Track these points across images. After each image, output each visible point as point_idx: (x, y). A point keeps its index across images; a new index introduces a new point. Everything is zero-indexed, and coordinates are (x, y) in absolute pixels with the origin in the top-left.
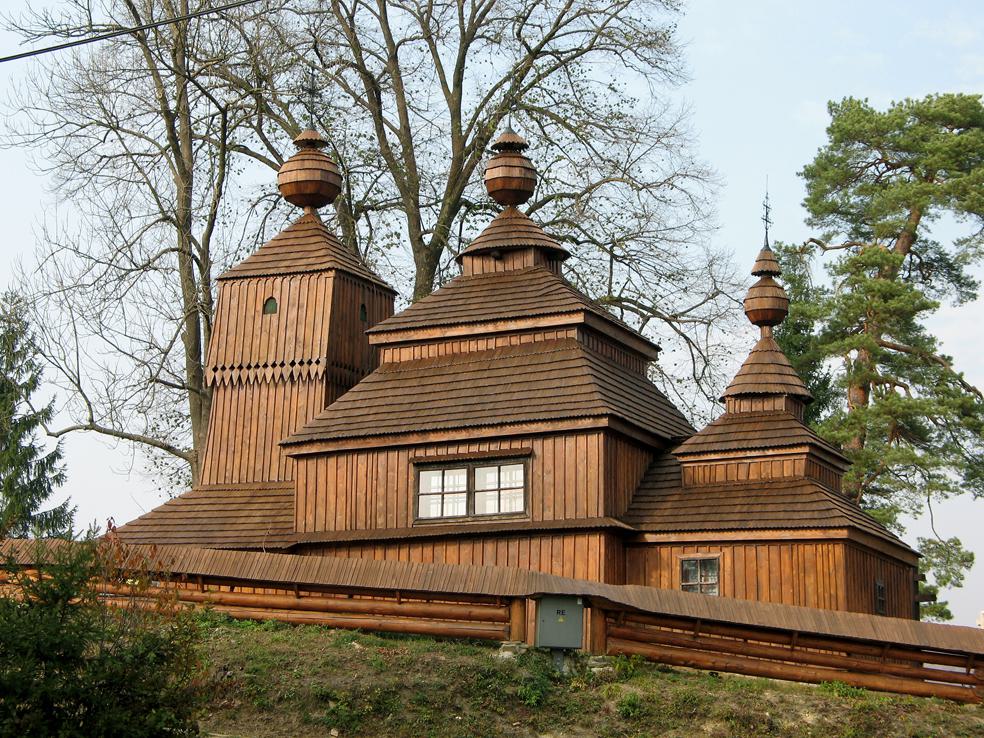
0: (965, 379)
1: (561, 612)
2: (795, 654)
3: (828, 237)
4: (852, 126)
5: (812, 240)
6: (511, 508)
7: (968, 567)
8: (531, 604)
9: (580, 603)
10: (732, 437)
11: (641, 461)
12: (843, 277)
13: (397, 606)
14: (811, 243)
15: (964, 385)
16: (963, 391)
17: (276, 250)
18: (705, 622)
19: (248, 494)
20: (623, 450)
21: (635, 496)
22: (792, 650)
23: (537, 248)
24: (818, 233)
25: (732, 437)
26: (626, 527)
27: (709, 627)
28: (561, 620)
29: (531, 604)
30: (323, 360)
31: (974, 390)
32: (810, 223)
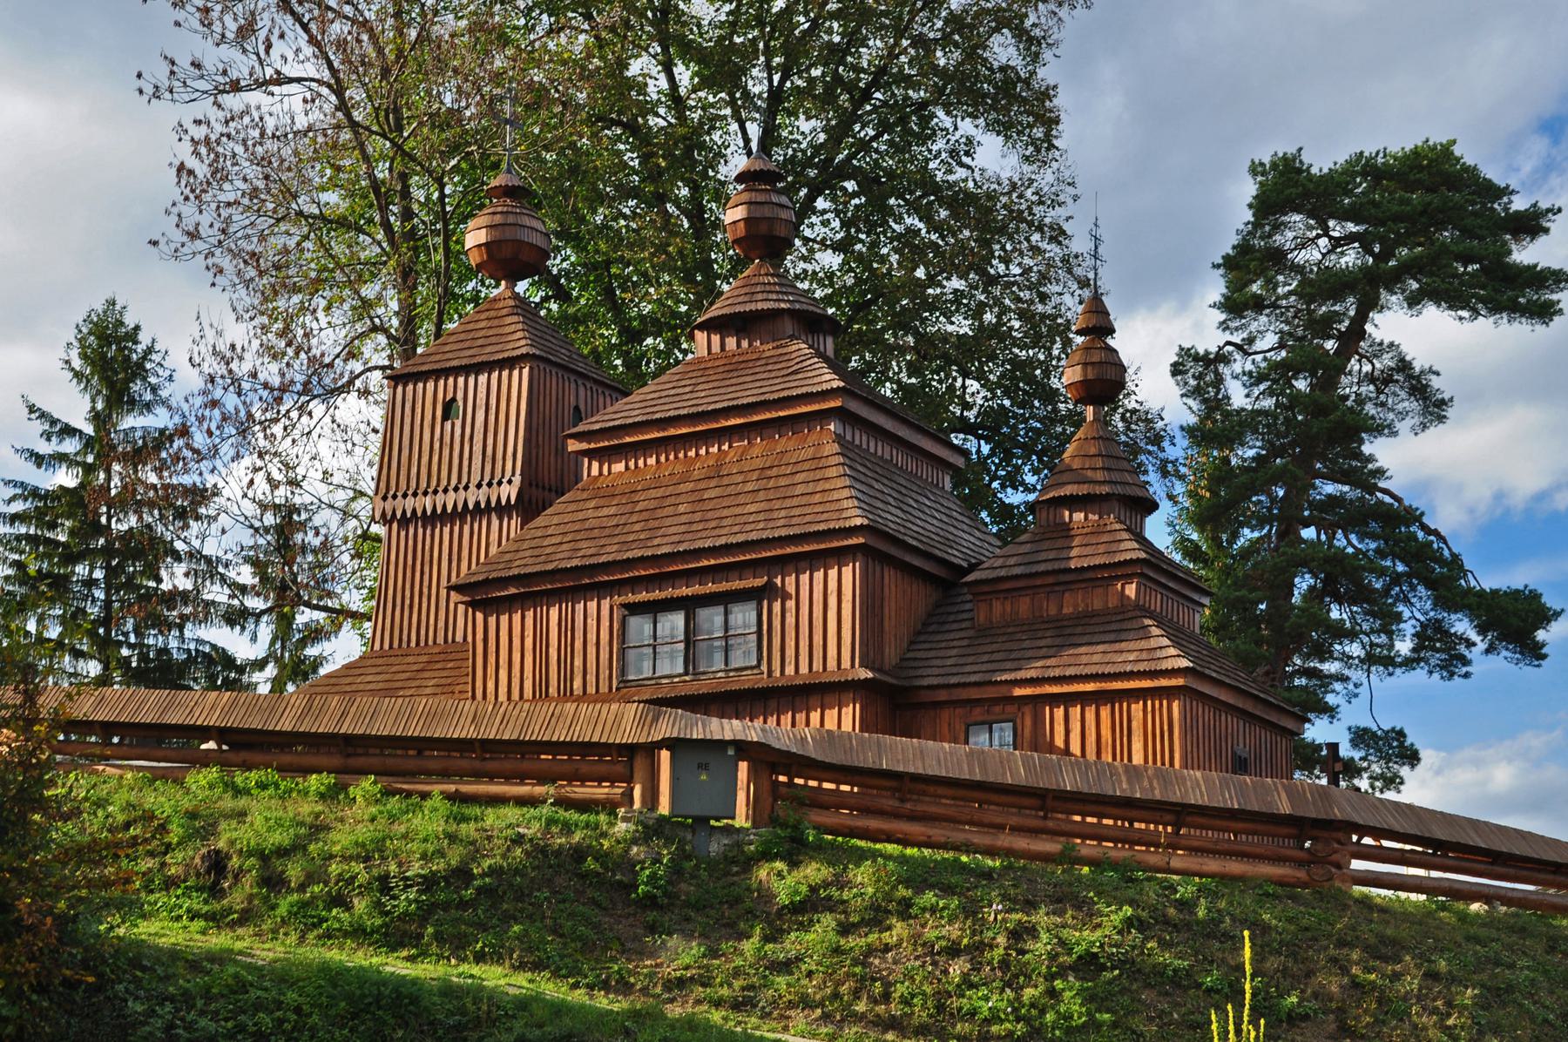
0: (1425, 520)
1: (703, 767)
2: (1050, 824)
3: (1251, 340)
4: (1286, 189)
5: (1229, 343)
6: (971, 771)
7: (1413, 766)
8: (665, 755)
9: (731, 752)
10: (1043, 556)
11: (921, 597)
12: (1262, 387)
13: (477, 764)
14: (1230, 348)
15: (1424, 527)
16: (1420, 535)
17: (463, 336)
18: (916, 778)
19: (425, 658)
20: (890, 577)
21: (912, 643)
22: (1045, 818)
23: (791, 313)
25: (1043, 556)
26: (894, 681)
27: (923, 787)
28: (704, 777)
29: (665, 755)
30: (517, 479)
31: (1436, 533)
32: (1224, 326)
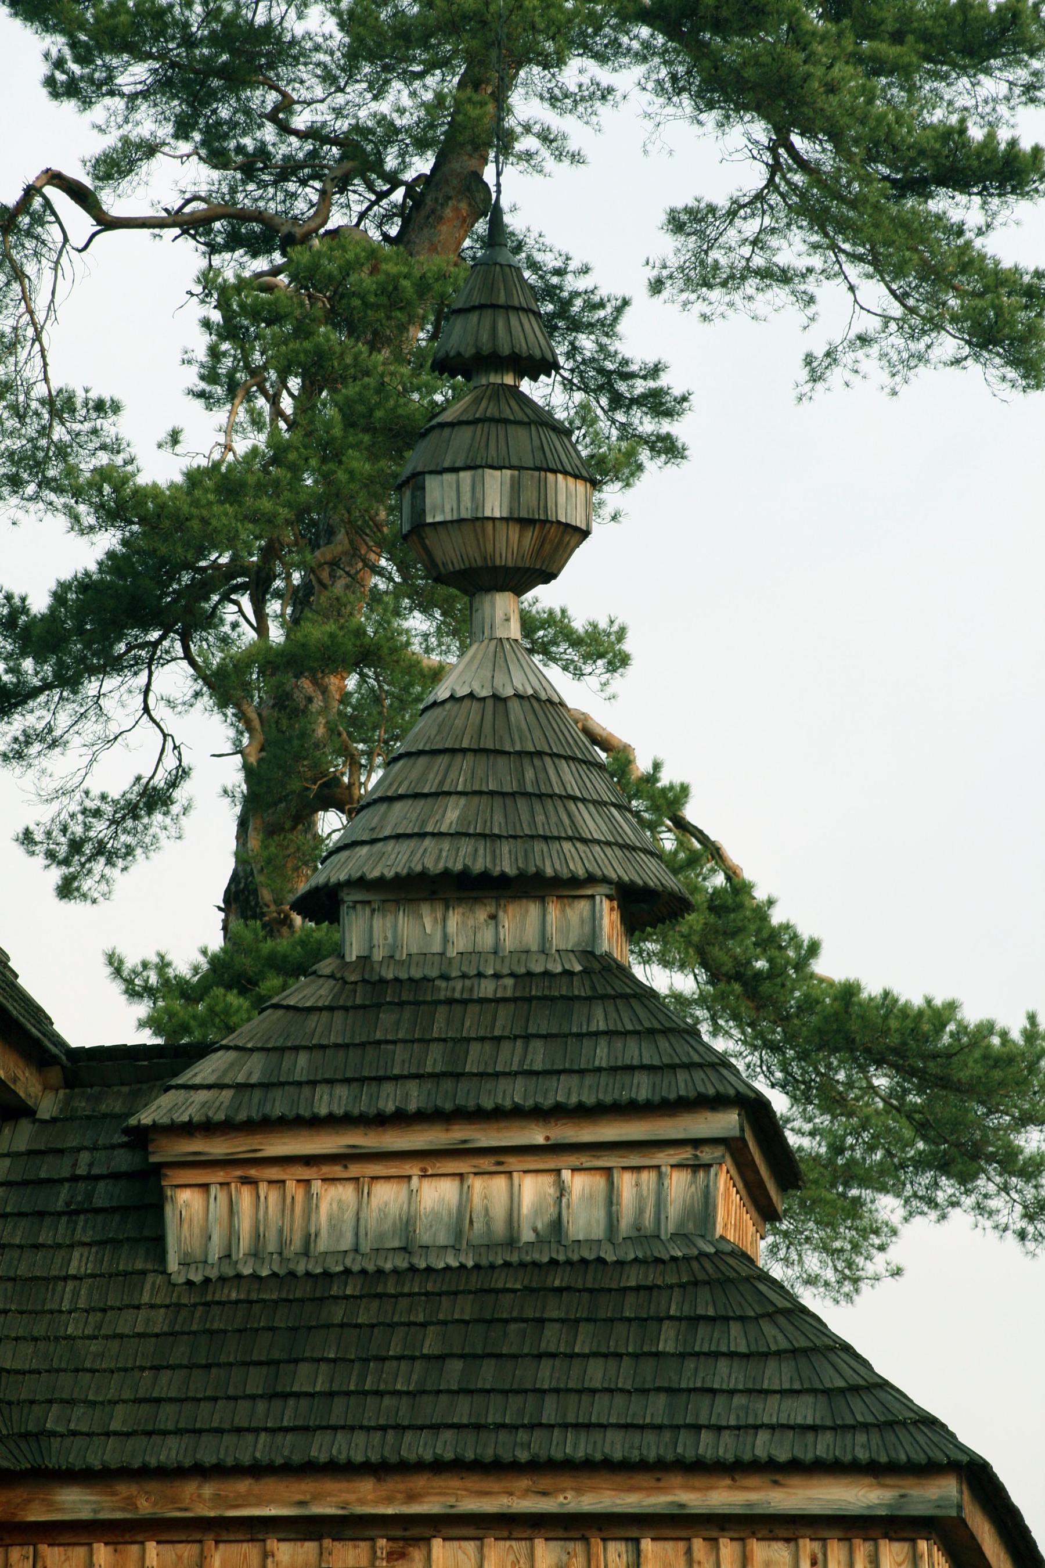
5: (56, 178)
14: (53, 193)
24: (75, 136)
